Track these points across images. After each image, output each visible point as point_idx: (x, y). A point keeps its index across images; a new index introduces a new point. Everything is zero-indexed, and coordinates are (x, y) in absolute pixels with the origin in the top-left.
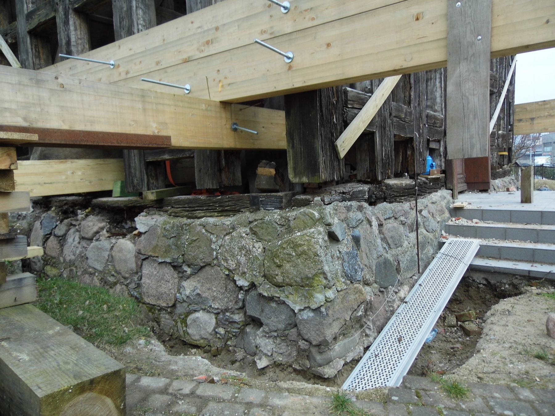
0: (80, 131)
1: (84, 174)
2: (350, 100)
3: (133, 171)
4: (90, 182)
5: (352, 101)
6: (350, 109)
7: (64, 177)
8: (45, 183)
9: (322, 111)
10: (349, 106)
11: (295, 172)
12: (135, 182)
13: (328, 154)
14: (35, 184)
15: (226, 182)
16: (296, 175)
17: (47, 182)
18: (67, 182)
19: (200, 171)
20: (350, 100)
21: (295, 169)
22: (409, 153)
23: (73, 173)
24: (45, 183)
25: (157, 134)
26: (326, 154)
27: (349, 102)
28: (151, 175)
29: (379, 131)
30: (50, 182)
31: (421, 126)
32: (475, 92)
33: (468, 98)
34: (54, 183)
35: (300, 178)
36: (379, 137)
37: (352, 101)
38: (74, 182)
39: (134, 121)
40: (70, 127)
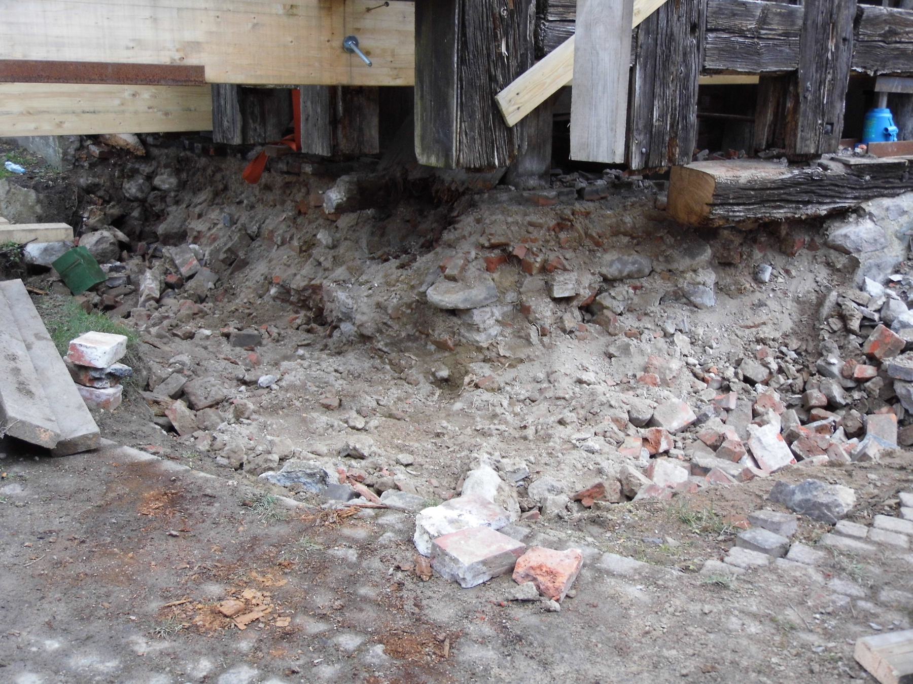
0: (36, 62)
1: (154, 96)
2: (553, 6)
3: (222, 103)
4: (166, 114)
5: (563, 6)
6: (553, 24)
7: (117, 102)
8: (84, 112)
9: (464, 34)
10: (550, 19)
11: (422, 145)
12: (226, 124)
13: (478, 116)
14: (66, 113)
15: (344, 146)
16: (423, 150)
17: (87, 110)
18: (123, 112)
19: (307, 119)
20: (553, 6)
21: (423, 138)
22: (789, 105)
23: (134, 95)
24: (84, 112)
25: (178, 63)
26: (472, 116)
27: (551, 10)
28: (252, 113)
29: (644, 67)
30: (92, 109)
31: (831, 45)
32: (607, 45)
33: (598, 53)
34: (99, 112)
35: (428, 158)
36: (640, 77)
37: (563, 6)
38: (136, 113)
39: (133, 40)
40: (25, 56)
